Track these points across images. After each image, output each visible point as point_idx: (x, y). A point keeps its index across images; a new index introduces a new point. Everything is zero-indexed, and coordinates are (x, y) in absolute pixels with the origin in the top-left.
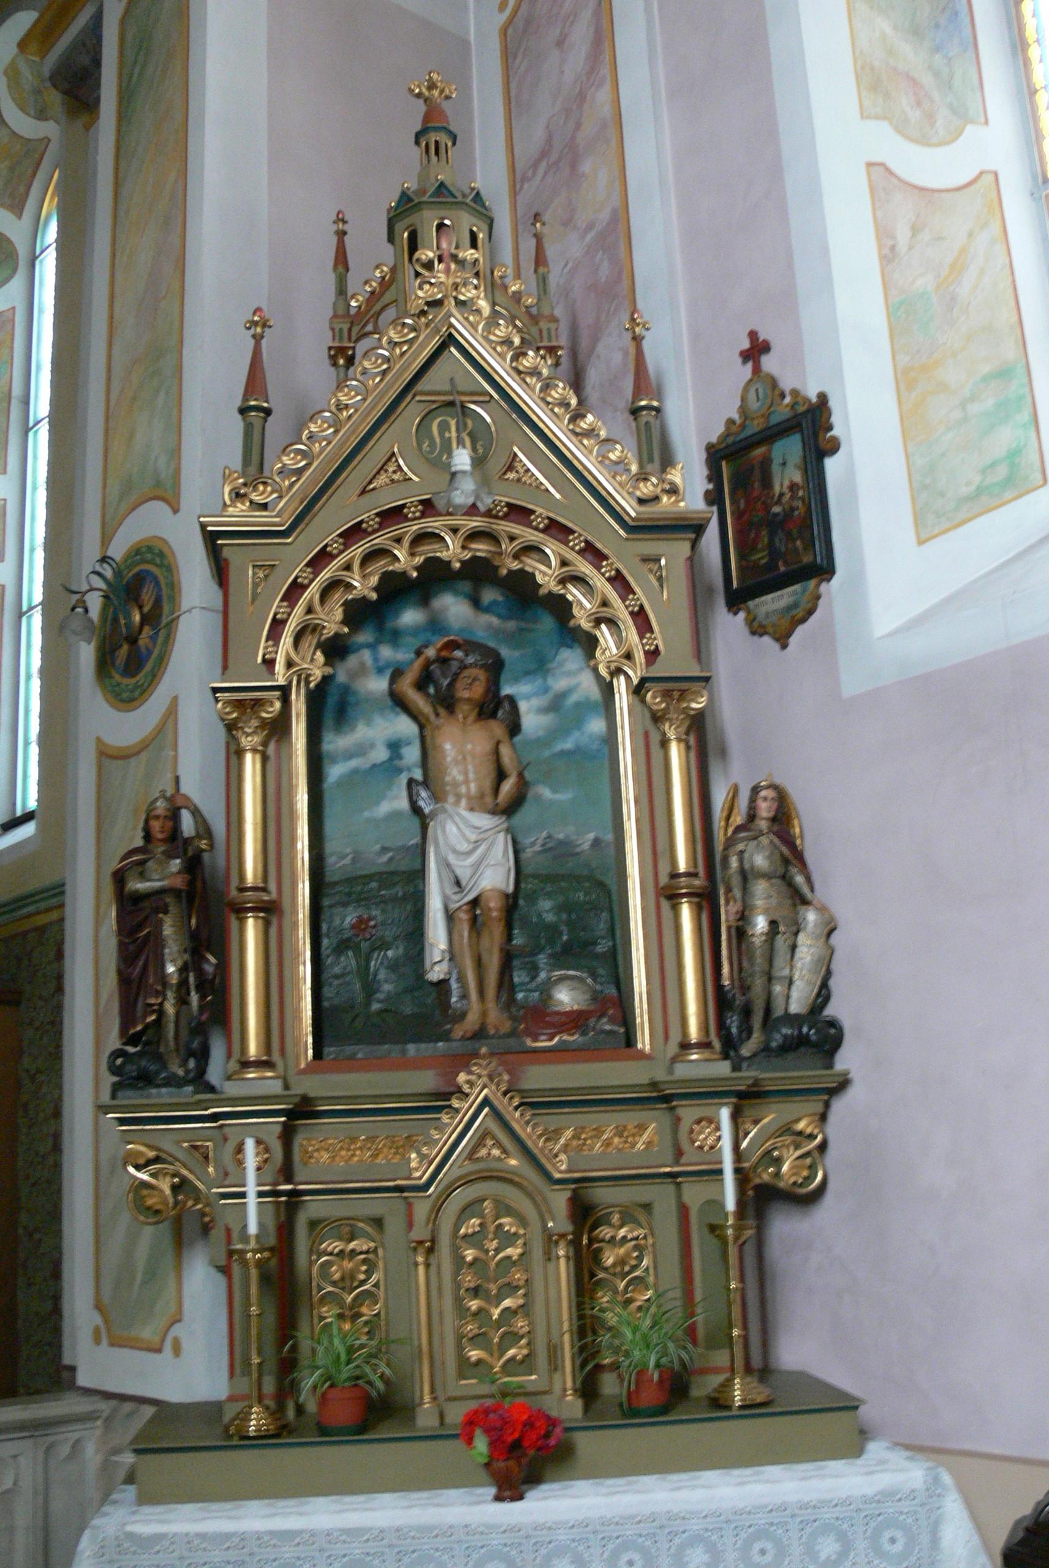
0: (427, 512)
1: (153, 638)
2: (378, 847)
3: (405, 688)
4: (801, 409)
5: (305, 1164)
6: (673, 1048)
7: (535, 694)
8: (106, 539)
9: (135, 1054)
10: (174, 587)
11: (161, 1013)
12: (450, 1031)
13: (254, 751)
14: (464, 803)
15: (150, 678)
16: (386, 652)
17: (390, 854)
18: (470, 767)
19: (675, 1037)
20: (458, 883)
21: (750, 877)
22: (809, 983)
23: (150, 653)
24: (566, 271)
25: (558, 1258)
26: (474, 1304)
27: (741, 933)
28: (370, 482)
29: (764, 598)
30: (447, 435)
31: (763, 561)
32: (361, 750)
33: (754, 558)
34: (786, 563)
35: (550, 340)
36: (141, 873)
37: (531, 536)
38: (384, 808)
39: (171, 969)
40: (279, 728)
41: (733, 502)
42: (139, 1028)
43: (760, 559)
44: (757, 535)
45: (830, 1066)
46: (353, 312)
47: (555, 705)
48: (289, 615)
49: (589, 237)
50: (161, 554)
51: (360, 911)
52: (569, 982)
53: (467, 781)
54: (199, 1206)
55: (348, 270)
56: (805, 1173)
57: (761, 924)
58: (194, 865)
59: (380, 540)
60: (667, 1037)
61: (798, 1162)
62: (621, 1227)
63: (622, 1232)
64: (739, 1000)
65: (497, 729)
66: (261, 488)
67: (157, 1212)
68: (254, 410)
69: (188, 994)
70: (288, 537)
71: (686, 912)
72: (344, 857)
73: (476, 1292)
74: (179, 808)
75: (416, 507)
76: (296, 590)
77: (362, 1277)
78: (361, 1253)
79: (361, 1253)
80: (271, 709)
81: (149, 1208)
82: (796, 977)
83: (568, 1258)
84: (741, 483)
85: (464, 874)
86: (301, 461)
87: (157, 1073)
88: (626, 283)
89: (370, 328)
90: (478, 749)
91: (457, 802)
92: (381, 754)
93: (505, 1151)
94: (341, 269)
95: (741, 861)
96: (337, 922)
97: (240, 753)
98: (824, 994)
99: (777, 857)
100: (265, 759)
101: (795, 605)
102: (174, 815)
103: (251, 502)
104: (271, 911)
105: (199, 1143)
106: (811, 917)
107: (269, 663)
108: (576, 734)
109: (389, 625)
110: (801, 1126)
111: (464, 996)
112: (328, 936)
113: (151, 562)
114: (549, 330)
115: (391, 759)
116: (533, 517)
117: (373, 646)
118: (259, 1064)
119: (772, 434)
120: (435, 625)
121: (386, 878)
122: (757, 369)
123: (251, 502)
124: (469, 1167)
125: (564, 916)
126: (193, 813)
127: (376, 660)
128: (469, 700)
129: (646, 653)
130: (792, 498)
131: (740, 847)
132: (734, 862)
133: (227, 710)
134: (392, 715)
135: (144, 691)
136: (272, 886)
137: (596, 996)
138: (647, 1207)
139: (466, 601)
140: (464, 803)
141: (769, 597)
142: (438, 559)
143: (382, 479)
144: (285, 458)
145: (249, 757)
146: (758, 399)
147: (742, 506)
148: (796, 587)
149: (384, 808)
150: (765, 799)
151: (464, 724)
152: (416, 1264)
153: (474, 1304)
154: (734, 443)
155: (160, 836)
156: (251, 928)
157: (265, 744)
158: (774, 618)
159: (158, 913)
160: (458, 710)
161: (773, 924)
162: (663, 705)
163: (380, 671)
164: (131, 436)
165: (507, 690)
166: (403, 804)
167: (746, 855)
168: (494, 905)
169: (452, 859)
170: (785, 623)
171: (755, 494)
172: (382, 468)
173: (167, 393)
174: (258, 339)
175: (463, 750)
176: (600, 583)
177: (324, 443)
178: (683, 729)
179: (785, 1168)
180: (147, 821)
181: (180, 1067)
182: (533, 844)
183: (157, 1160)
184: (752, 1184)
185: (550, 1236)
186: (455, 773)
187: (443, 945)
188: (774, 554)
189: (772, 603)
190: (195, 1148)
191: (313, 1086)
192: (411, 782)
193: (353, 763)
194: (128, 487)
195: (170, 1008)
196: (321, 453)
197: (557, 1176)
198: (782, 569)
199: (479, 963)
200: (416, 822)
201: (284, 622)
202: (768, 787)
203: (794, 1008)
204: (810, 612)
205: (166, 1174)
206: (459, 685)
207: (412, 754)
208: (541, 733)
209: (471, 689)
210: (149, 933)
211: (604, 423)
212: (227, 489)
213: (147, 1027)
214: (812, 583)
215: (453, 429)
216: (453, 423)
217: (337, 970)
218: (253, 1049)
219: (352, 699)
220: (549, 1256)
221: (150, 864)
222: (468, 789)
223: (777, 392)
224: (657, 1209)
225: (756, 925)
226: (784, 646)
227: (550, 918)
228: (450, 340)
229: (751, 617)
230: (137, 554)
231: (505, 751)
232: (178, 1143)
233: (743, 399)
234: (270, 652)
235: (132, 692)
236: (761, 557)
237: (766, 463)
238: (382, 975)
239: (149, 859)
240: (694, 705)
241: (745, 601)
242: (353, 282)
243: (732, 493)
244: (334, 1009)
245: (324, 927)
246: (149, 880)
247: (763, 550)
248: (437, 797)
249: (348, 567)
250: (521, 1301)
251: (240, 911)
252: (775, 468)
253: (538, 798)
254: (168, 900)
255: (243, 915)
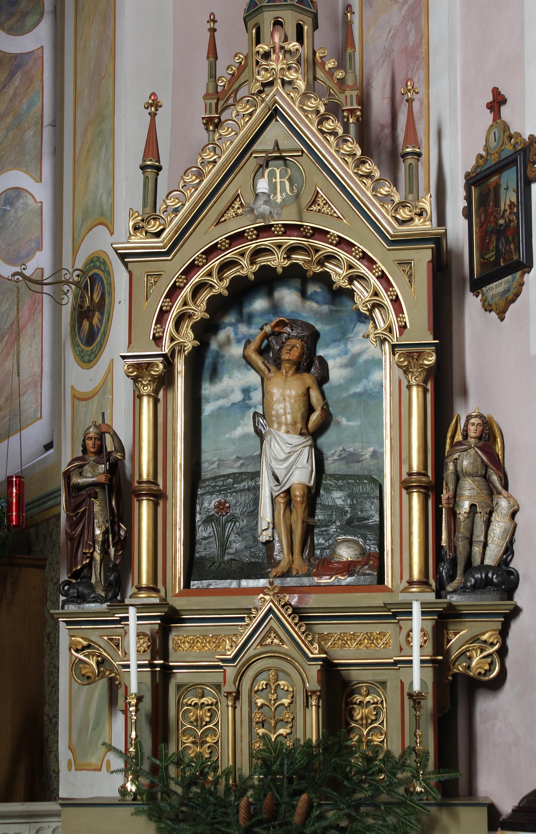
0: (261, 235)
1: (101, 321)
2: (234, 457)
3: (250, 353)
4: (519, 148)
5: (176, 651)
6: (404, 584)
7: (339, 355)
8: (75, 252)
9: (75, 583)
10: (111, 285)
11: (92, 558)
12: (270, 572)
13: (149, 395)
14: (284, 427)
15: (99, 347)
16: (243, 329)
17: (242, 462)
18: (288, 404)
19: (406, 577)
20: (277, 479)
21: (461, 475)
22: (498, 545)
23: (99, 330)
24: (390, 35)
25: (312, 706)
26: (261, 731)
27: (453, 513)
28: (223, 216)
29: (491, 285)
30: (274, 180)
31: (492, 259)
32: (225, 395)
33: (487, 257)
34: (505, 260)
35: (352, 105)
36: (81, 473)
37: (329, 248)
38: (239, 432)
39: (98, 532)
40: (166, 381)
41: (478, 216)
42: (79, 567)
43: (490, 257)
44: (490, 239)
45: (511, 598)
46: (220, 89)
47: (352, 362)
48: (171, 307)
49: (406, 8)
50: (104, 263)
51: (220, 498)
52: (346, 543)
53: (285, 414)
54: (113, 675)
55: (216, 58)
56: (487, 667)
57: (466, 505)
58: (115, 468)
59: (229, 255)
60: (401, 578)
61: (483, 660)
62: (367, 695)
63: (368, 699)
64: (449, 555)
65: (308, 379)
66: (152, 222)
67: (88, 677)
68: (151, 167)
69: (109, 547)
70: (169, 256)
71: (416, 498)
72: (213, 463)
73: (263, 724)
74: (104, 433)
75: (252, 232)
76: (174, 290)
77: (208, 719)
78: (208, 705)
79: (208, 705)
80: (157, 369)
81: (83, 675)
82: (489, 542)
83: (318, 707)
84: (483, 202)
85: (280, 475)
86: (178, 203)
87: (89, 594)
88: (424, 47)
89: (231, 101)
90: (293, 393)
91: (279, 428)
92: (238, 397)
93: (281, 641)
94: (212, 59)
95: (456, 466)
96: (206, 505)
97: (140, 397)
98: (509, 550)
99: (479, 462)
100: (156, 401)
101: (508, 290)
102: (101, 437)
103: (147, 232)
104: (158, 497)
105: (114, 637)
106: (503, 503)
107: (158, 340)
108: (365, 381)
109: (246, 310)
110: (484, 637)
111: (281, 551)
112: (200, 514)
113: (96, 267)
114: (351, 96)
115: (244, 400)
116: (329, 236)
117: (234, 325)
118: (148, 589)
119: (501, 167)
120: (275, 308)
121: (237, 477)
122: (497, 115)
123: (147, 232)
124: (260, 649)
125: (349, 501)
126: (112, 436)
127: (236, 334)
128: (288, 360)
129: (400, 327)
130: (510, 213)
131: (456, 456)
132: (451, 467)
133: (131, 370)
134: (246, 370)
135: (96, 356)
136: (160, 481)
137: (363, 552)
138: (383, 684)
139: (296, 292)
140: (284, 427)
141: (493, 285)
142: (268, 266)
143: (231, 213)
144: (168, 202)
145: (145, 399)
146: (495, 141)
147: (483, 220)
148: (509, 277)
149: (239, 432)
150: (473, 424)
151: (286, 376)
152: (228, 706)
153: (261, 731)
154: (481, 173)
155: (92, 450)
156: (145, 507)
157: (156, 391)
158: (496, 299)
159: (90, 498)
160: (282, 368)
161: (473, 506)
162: (406, 363)
163: (239, 341)
164: (88, 179)
165: (320, 352)
166: (251, 429)
167: (459, 462)
168: (298, 493)
169: (274, 464)
170: (502, 303)
171: (490, 210)
172: (230, 206)
173: (107, 149)
174: (153, 115)
175: (286, 394)
176: (373, 280)
177: (193, 190)
178: (421, 378)
179: (474, 663)
180: (84, 441)
181: (103, 591)
182: (333, 455)
183: (89, 646)
184: (451, 673)
185: (307, 692)
186: (279, 408)
187: (269, 519)
188: (498, 254)
189: (496, 288)
190: (111, 640)
191: (179, 603)
192: (255, 414)
193: (220, 403)
194: (86, 214)
195: (97, 556)
196: (191, 196)
197: (311, 656)
198: (502, 264)
199: (290, 532)
200: (258, 439)
201: (168, 312)
202: (476, 416)
203: (488, 561)
204: (517, 295)
205: (93, 656)
206: (284, 351)
207: (257, 396)
208: (342, 381)
209: (292, 351)
210: (85, 510)
211: (379, 168)
212: (131, 224)
213: (84, 567)
214: (519, 274)
215: (278, 175)
216: (278, 172)
217: (205, 534)
218: (144, 581)
219: (221, 360)
220: (307, 705)
221: (86, 467)
222: (286, 419)
223: (507, 134)
224: (389, 685)
225: (462, 507)
226: (502, 319)
227: (339, 502)
228: (275, 113)
229: (484, 298)
230: (91, 262)
231: (314, 395)
232: (101, 636)
233: (487, 141)
234: (159, 332)
235: (90, 356)
236: (491, 256)
237: (497, 187)
238: (232, 538)
239: (85, 465)
240: (426, 362)
241: (481, 288)
242: (221, 70)
243: (477, 211)
244: (202, 558)
245: (198, 508)
246: (86, 477)
247: (493, 251)
248: (270, 425)
249: (210, 274)
250: (288, 731)
251: (139, 496)
252: (502, 191)
253: (338, 423)
254: (97, 490)
255: (140, 498)
